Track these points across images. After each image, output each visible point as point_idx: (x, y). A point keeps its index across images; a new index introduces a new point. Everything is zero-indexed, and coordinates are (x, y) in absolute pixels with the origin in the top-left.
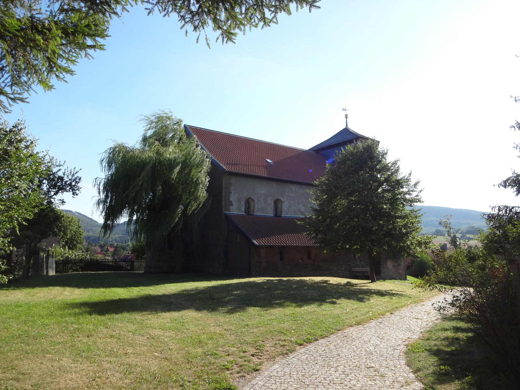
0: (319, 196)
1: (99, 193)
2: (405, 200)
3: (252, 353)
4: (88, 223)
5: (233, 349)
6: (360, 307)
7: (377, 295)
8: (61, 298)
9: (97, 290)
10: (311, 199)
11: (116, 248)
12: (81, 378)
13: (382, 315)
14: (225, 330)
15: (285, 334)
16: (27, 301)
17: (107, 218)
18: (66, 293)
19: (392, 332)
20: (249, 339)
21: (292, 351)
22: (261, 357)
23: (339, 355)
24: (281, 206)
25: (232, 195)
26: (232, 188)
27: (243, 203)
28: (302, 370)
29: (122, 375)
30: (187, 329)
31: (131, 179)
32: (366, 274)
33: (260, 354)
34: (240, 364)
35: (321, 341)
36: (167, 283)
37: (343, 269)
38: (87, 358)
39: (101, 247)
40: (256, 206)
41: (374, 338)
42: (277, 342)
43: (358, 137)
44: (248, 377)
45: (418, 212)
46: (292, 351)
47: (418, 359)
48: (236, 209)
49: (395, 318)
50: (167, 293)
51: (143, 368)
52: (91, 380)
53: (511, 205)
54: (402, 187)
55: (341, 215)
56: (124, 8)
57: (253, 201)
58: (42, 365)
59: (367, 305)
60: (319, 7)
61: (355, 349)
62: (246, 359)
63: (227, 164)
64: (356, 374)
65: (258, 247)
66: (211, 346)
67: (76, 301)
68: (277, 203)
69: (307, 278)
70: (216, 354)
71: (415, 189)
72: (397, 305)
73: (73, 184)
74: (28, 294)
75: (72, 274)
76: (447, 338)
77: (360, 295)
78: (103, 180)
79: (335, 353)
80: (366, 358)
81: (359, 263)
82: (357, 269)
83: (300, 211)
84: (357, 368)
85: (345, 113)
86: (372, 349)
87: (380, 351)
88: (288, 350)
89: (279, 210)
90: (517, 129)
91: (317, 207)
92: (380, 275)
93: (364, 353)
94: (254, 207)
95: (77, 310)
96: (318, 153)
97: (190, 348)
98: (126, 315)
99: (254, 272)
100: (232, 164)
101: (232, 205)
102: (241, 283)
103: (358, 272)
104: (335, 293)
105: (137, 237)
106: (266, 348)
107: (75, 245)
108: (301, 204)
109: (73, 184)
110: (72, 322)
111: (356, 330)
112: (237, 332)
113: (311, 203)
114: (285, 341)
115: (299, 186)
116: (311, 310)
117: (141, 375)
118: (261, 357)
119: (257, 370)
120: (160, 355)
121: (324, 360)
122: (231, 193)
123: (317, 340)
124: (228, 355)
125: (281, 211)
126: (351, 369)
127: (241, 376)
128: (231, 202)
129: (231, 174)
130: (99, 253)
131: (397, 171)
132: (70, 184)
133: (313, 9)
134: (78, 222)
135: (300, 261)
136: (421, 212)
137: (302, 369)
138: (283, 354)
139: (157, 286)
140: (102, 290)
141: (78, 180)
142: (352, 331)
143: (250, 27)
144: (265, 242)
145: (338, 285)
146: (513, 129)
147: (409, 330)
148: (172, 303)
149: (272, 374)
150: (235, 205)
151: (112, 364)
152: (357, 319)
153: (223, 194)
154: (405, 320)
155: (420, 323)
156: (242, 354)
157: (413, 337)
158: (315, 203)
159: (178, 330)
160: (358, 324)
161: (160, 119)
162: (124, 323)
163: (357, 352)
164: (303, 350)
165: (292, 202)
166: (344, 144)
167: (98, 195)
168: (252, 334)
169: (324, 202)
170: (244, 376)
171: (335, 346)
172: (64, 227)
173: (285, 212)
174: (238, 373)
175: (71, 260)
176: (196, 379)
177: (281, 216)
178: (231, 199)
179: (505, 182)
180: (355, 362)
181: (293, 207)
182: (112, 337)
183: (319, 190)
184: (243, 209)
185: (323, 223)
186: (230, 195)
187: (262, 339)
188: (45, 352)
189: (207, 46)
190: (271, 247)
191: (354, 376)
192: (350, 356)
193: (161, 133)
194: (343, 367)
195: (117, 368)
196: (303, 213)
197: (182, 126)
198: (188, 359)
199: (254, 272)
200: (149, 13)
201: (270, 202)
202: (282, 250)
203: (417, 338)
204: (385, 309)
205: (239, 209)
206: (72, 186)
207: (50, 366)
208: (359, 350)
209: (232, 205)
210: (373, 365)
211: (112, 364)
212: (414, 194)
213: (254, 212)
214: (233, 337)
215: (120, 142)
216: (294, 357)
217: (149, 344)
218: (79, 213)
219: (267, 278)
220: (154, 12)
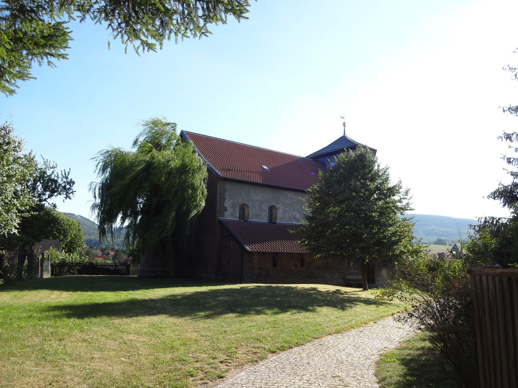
0: (311, 204)
1: (95, 197)
2: (397, 208)
3: (222, 359)
4: (90, 226)
5: (203, 355)
6: (345, 316)
7: (365, 303)
8: (45, 301)
9: (85, 293)
10: (305, 206)
11: (117, 251)
12: (38, 381)
13: (365, 324)
14: (202, 336)
15: (261, 341)
16: (11, 303)
17: (103, 221)
18: (54, 296)
19: (370, 341)
20: (223, 346)
21: (263, 359)
22: (229, 364)
23: (309, 364)
24: (276, 213)
25: (226, 201)
26: (227, 194)
27: (237, 209)
28: (267, 378)
29: (81, 380)
30: (162, 334)
31: (130, 182)
32: (360, 282)
33: (230, 361)
34: (205, 371)
35: (295, 349)
36: (157, 288)
37: (336, 276)
38: (50, 362)
39: (103, 250)
40: (251, 212)
41: (350, 347)
42: (250, 349)
43: (354, 146)
44: (211, 384)
45: (410, 221)
46: (262, 359)
47: (388, 369)
48: (230, 214)
49: (377, 327)
50: (155, 298)
51: (106, 373)
52: (48, 384)
53: (497, 216)
54: (394, 195)
55: (328, 223)
56: (71, 17)
57: (248, 207)
58: (3, 369)
59: (352, 313)
60: (248, 18)
61: (327, 357)
62: (213, 365)
63: (222, 169)
64: (320, 383)
65: (250, 253)
66: (180, 352)
67: (59, 304)
68: (272, 209)
69: (300, 286)
70: (184, 360)
71: (406, 197)
72: (384, 314)
73: (68, 187)
74: (15, 296)
75: (65, 277)
76: (423, 348)
77: (340, 303)
78: (98, 185)
79: (305, 362)
80: (335, 367)
81: (352, 271)
82: (350, 277)
83: (295, 218)
84: (322, 377)
85: (343, 121)
86: (344, 357)
87: (352, 360)
88: (259, 357)
89: (274, 217)
90: (504, 140)
91: (310, 215)
92: (375, 283)
93: (335, 361)
94: (249, 213)
95: (57, 313)
96: (316, 160)
97: (160, 354)
98: (105, 319)
99: (246, 279)
100: (228, 170)
101: (226, 210)
102: (231, 289)
103: (352, 280)
104: (323, 300)
105: (129, 241)
106: (238, 356)
107: (74, 248)
108: (295, 211)
109: (68, 187)
110: (49, 326)
111: (334, 338)
112: (213, 339)
113: (304, 210)
114: (258, 348)
115: (294, 193)
116: (301, 318)
117: (101, 380)
118: (229, 364)
119: (222, 377)
120: (127, 360)
121: (293, 369)
122: (226, 198)
123: (292, 348)
124: (197, 361)
125: (276, 218)
126: (316, 378)
127: (203, 383)
128: (226, 207)
129: (226, 180)
130: (100, 257)
131: (387, 179)
132: (64, 187)
133: (242, 20)
134: (79, 226)
135: (293, 268)
136: (413, 221)
137: (267, 377)
138: (252, 362)
139: (146, 291)
140: (90, 293)
141: (71, 183)
142: (329, 340)
143: (182, 38)
144: (258, 248)
145: (328, 292)
146: (501, 139)
147: (388, 339)
148: (155, 308)
149: (235, 382)
150: (230, 210)
151: (74, 368)
152: (338, 327)
153: (218, 200)
154: (386, 329)
155: (401, 332)
156: (212, 361)
157: (390, 347)
158: (308, 211)
159: (153, 335)
160: (338, 332)
161: (155, 123)
162: (99, 327)
163: (328, 361)
164: (275, 358)
165: (287, 209)
166: (337, 152)
167: (94, 199)
168: (228, 341)
169: (318, 209)
170: (206, 383)
171: (308, 354)
172: (64, 230)
173: (280, 219)
174: (202, 380)
175: (68, 263)
176: (157, 385)
177: (276, 223)
178: (226, 205)
179: (495, 193)
180: (323, 371)
181: (288, 214)
182: (84, 341)
183: (312, 197)
184: (237, 215)
185: (317, 229)
186: (224, 201)
187: (234, 345)
188: (12, 354)
189: (136, 54)
190: (264, 253)
191: (317, 385)
192: (320, 365)
193: (156, 138)
194: (309, 375)
195: (78, 372)
196: (298, 220)
197: (178, 133)
198: (154, 365)
199: (246, 279)
200: (81, 21)
201: (265, 208)
202: (275, 257)
203: (394, 347)
204: (370, 318)
205: (233, 215)
206: (66, 188)
207: (10, 370)
208: (331, 359)
209: (226, 210)
210: (340, 374)
211: (74, 368)
212: (405, 202)
213: (248, 218)
214: (207, 343)
215: (116, 147)
216: (262, 365)
217: (119, 349)
218: (81, 216)
219: (258, 285)
220: (86, 20)
